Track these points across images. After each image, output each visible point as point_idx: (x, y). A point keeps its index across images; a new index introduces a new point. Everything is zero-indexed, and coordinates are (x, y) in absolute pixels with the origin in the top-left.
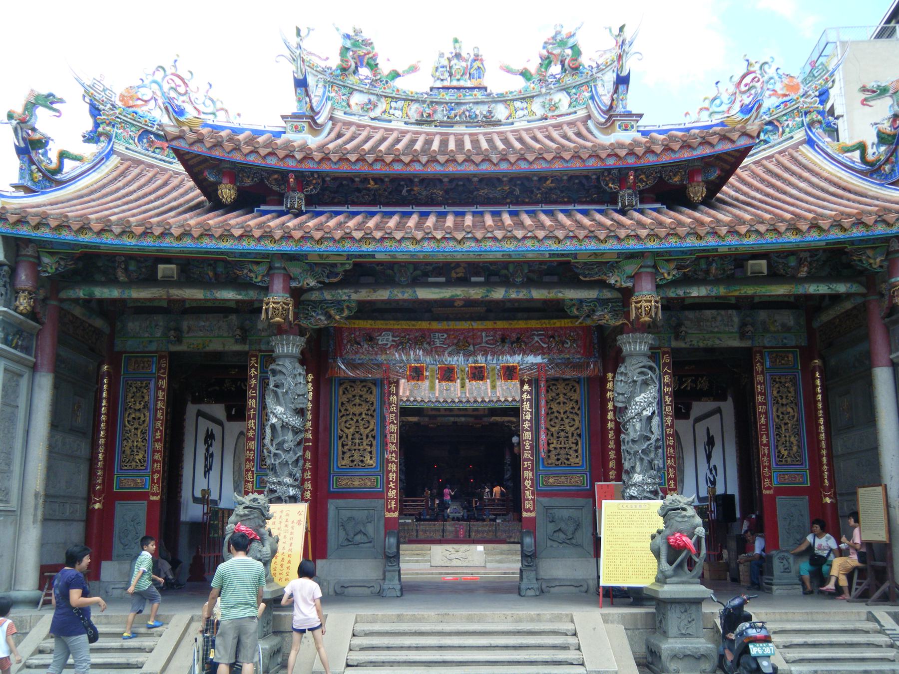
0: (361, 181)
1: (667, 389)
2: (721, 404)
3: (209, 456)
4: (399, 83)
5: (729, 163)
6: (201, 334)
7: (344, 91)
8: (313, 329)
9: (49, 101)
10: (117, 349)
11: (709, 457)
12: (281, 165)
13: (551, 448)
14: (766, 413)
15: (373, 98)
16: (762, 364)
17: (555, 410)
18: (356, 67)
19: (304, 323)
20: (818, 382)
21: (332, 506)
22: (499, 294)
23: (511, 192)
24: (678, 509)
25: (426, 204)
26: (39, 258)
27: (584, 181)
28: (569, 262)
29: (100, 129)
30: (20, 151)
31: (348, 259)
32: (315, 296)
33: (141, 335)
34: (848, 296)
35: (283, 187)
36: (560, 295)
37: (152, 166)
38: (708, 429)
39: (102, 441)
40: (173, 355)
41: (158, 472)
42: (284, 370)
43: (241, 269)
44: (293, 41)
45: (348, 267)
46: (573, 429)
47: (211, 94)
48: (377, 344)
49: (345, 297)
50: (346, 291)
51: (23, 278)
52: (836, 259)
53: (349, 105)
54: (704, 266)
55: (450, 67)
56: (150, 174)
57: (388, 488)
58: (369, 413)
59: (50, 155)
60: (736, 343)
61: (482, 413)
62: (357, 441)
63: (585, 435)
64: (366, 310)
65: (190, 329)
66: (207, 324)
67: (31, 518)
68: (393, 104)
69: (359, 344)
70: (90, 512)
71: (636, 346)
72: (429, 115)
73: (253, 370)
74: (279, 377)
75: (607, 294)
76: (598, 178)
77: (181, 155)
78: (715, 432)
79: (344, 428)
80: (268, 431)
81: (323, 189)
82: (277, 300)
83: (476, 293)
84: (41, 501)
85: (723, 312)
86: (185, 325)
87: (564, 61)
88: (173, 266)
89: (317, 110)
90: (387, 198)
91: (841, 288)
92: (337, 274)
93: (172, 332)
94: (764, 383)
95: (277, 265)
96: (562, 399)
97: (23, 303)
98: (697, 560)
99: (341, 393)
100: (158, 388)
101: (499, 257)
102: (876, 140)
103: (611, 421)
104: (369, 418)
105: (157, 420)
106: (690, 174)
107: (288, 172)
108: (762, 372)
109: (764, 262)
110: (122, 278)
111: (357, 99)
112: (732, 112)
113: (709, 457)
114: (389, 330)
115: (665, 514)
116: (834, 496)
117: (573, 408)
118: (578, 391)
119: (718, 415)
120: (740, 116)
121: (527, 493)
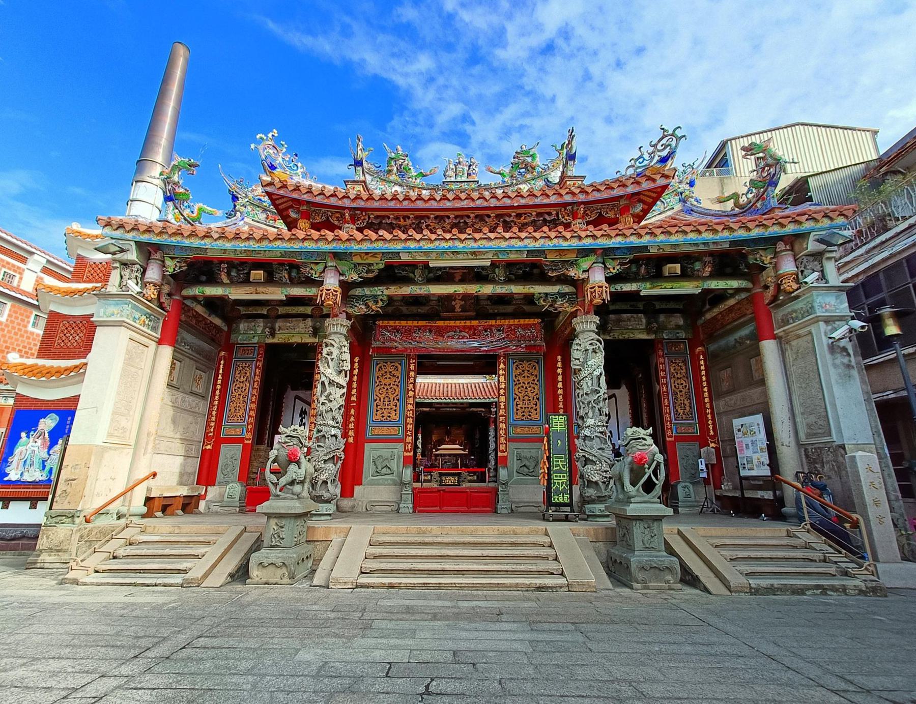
6: (287, 331)
12: (340, 203)
20: (702, 362)
21: (22, 287)
26: (163, 262)
34: (738, 291)
36: (532, 291)
41: (251, 424)
42: (333, 343)
57: (406, 435)
60: (644, 336)
62: (387, 403)
65: (280, 328)
70: (204, 452)
85: (635, 316)
95: (330, 264)
96: (526, 374)
98: (657, 482)
104: (395, 387)
108: (663, 356)
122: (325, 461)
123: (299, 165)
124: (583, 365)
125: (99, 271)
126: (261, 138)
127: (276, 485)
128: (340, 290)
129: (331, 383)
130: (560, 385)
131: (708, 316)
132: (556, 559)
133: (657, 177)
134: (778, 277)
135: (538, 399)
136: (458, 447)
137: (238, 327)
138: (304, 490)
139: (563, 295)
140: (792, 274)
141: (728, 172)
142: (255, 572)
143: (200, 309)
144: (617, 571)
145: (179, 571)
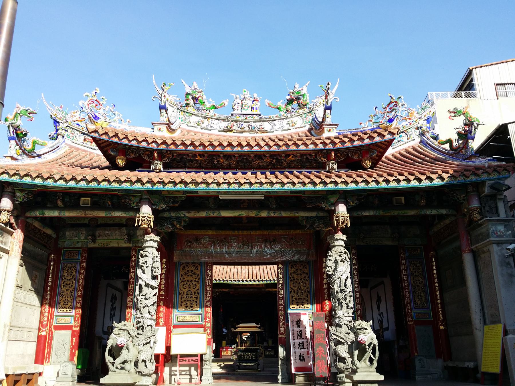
0: (193, 156)
1: (354, 267)
3: (113, 309)
6: (106, 238)
8: (165, 233)
10: (60, 246)
11: (379, 308)
13: (294, 299)
14: (407, 280)
16: (404, 254)
17: (295, 278)
20: (434, 264)
23: (271, 162)
24: (362, 328)
25: (227, 169)
27: (309, 157)
28: (300, 196)
29: (59, 132)
31: (183, 194)
32: (166, 215)
35: (151, 158)
36: (297, 215)
37: (85, 151)
38: (378, 293)
40: (91, 250)
41: (78, 314)
45: (184, 198)
46: (305, 288)
48: (201, 243)
49: (182, 215)
50: (183, 212)
55: (242, 104)
58: (197, 280)
60: (390, 243)
61: (261, 286)
62: (189, 296)
65: (100, 235)
66: (110, 232)
69: (191, 242)
73: (133, 257)
74: (146, 259)
75: (322, 214)
76: (316, 156)
81: (173, 160)
86: (97, 233)
88: (89, 199)
89: (172, 122)
90: (206, 165)
91: (444, 212)
92: (178, 202)
93: (90, 237)
94: (405, 264)
96: (299, 272)
99: (181, 269)
102: (457, 138)
103: (326, 284)
104: (196, 283)
105: (79, 285)
106: (360, 155)
108: (404, 258)
110: (60, 204)
113: (379, 308)
117: (305, 277)
118: (199, 268)
119: (383, 285)
121: (281, 324)
122: (144, 345)
123: (116, 113)
124: (335, 269)
126: (87, 96)
127: (113, 364)
128: (152, 217)
129: (147, 285)
131: (435, 229)
133: (386, 133)
134: (470, 209)
136: (254, 325)
138: (130, 366)
140: (477, 209)
141: (474, 96)
143: (36, 224)
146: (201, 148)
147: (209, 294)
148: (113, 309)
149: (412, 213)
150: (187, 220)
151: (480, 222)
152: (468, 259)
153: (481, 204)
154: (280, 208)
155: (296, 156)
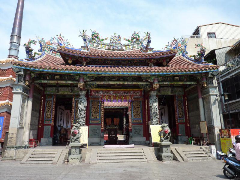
2: (165, 107)
3: (61, 117)
4: (104, 41)
5: (171, 58)
7: (92, 43)
9: (34, 42)
15: (98, 45)
18: (95, 38)
19: (86, 88)
20: (186, 102)
22: (126, 83)
26: (31, 74)
29: (42, 49)
30: (27, 52)
32: (88, 83)
33: (51, 91)
34: (193, 85)
36: (138, 83)
37: (53, 57)
39: (41, 113)
40: (57, 95)
43: (74, 77)
44: (82, 32)
45: (96, 77)
47: (68, 41)
51: (27, 78)
52: (191, 77)
53: (93, 45)
54: (166, 78)
56: (52, 58)
59: (33, 53)
60: (170, 94)
63: (142, 112)
64: (99, 86)
67: (27, 129)
68: (103, 46)
70: (39, 128)
71: (154, 94)
72: (110, 48)
75: (148, 83)
76: (145, 60)
77: (61, 54)
78: (163, 112)
79: (92, 110)
80: (78, 111)
82: (81, 84)
83: (121, 83)
84: (29, 125)
86: (59, 89)
87: (136, 38)
88: (59, 76)
91: (193, 83)
97: (27, 83)
100: (54, 102)
101: (127, 75)
106: (163, 59)
107: (83, 57)
109: (178, 78)
111: (95, 45)
112: (172, 48)
114: (102, 90)
115: (162, 127)
116: (190, 124)
119: (163, 109)
120: (173, 49)
124: (152, 105)
125: (5, 74)
129: (82, 110)
130: (146, 102)
132: (145, 156)
135: (140, 112)
137: (47, 89)
139: (147, 85)
141: (200, 37)
142: (70, 160)
144: (159, 158)
145: (51, 161)
146: (102, 57)
147: (103, 113)
148: (61, 117)
149: (181, 83)
150: (97, 85)
151: (206, 87)
152: (200, 100)
153: (207, 80)
154: (132, 81)
155: (138, 61)
